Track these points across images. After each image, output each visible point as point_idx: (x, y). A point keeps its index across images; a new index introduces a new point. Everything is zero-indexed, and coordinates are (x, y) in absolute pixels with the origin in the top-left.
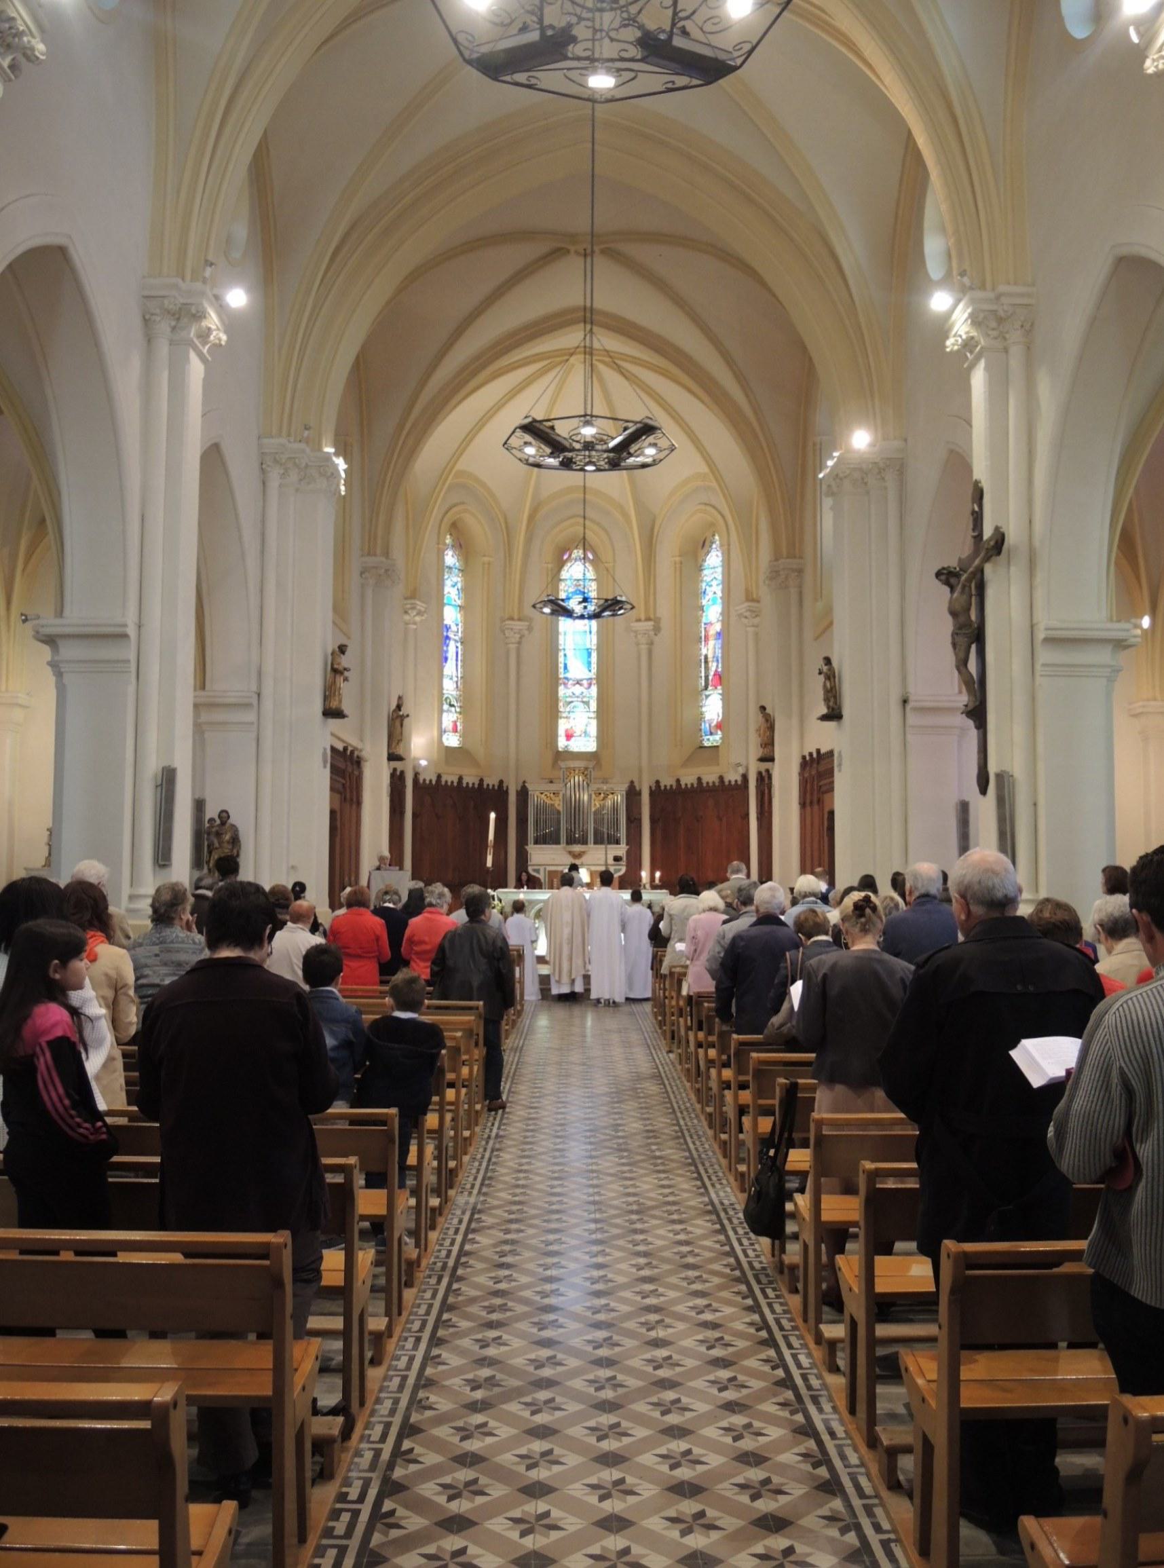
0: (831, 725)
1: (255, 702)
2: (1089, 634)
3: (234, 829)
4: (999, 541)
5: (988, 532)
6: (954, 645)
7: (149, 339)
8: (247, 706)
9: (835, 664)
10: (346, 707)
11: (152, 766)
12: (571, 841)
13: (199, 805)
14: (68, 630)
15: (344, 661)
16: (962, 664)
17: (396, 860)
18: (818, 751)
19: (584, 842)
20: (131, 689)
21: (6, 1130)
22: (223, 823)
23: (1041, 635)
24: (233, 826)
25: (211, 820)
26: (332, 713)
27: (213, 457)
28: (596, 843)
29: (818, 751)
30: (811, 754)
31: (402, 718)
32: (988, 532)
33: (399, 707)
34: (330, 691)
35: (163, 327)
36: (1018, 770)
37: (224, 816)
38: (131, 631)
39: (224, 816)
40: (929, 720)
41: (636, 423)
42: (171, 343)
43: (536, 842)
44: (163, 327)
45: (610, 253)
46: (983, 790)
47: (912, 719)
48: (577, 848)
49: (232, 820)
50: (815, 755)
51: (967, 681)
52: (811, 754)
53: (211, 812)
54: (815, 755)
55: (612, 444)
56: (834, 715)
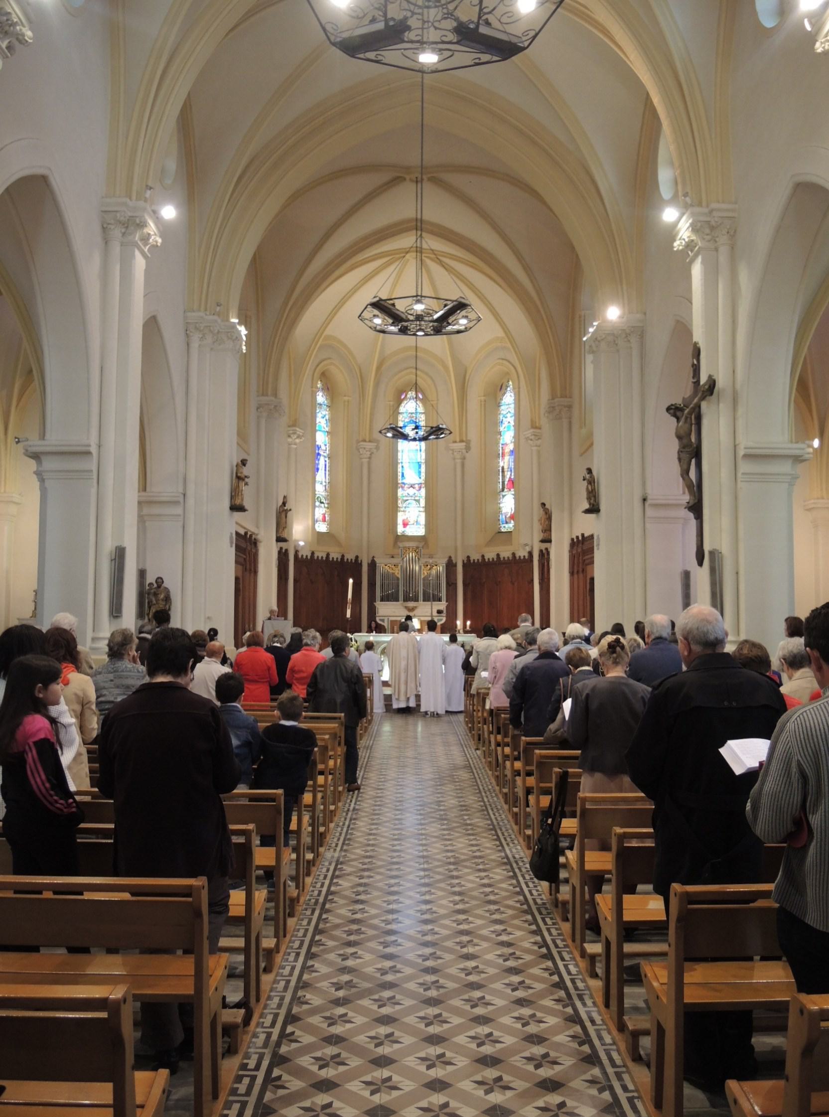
3: (167, 591)
4: (712, 385)
5: (703, 379)
7: (106, 242)
9: (595, 473)
10: (246, 504)
12: (407, 599)
13: (142, 574)
14: (48, 449)
15: (245, 471)
16: (685, 473)
18: (583, 535)
19: (416, 600)
20: (94, 491)
21: (5, 805)
22: (159, 587)
23: (741, 453)
26: (236, 508)
27: (152, 325)
29: (583, 535)
30: (577, 537)
31: (286, 511)
32: (703, 379)
33: (284, 504)
34: (235, 493)
35: (116, 232)
36: (725, 549)
37: (160, 581)
38: (94, 449)
39: (160, 581)
40: (662, 513)
41: (453, 301)
43: (382, 600)
45: (437, 181)
46: (700, 564)
47: (650, 512)
48: (411, 604)
51: (689, 485)
52: (577, 537)
53: (150, 579)
55: (436, 316)
56: (594, 509)
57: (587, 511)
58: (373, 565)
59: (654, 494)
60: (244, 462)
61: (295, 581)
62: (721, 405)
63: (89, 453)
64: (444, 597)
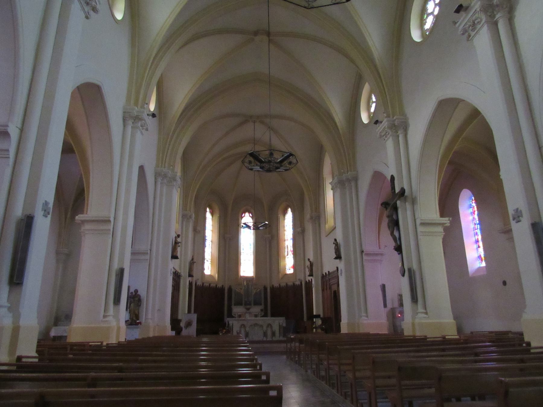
0: (338, 260)
1: (149, 252)
2: (434, 222)
3: (139, 296)
4: (403, 191)
5: (397, 190)
6: (389, 228)
7: (125, 126)
8: (145, 253)
9: (338, 241)
10: (179, 255)
11: (116, 266)
12: (246, 305)
13: (129, 287)
14: (88, 219)
15: (179, 240)
16: (392, 234)
17: (189, 311)
18: (329, 272)
19: (250, 304)
20: (110, 241)
21: (371, 333)
22: (136, 294)
23: (418, 222)
24: (139, 295)
25: (132, 293)
26: (174, 257)
27: (141, 168)
28: (254, 305)
29: (329, 272)
30: (326, 273)
31: (194, 263)
32: (397, 190)
33: (193, 259)
34: (174, 249)
35: (130, 123)
36: (415, 267)
37: (136, 291)
38: (112, 219)
39: (136, 291)
40: (369, 258)
41: (287, 153)
42: (132, 127)
43: (235, 305)
44: (130, 123)
45: (262, 122)
46: (403, 275)
47: (365, 257)
48: (248, 307)
49: (139, 293)
50: (327, 273)
51: (395, 239)
52: (326, 273)
53: (132, 290)
54: (327, 273)
55: (279, 160)
56: (338, 257)
57: (336, 258)
58: (230, 290)
59: (367, 248)
60: (178, 236)
61: (195, 296)
62: (407, 203)
63: (109, 221)
64: (263, 304)
